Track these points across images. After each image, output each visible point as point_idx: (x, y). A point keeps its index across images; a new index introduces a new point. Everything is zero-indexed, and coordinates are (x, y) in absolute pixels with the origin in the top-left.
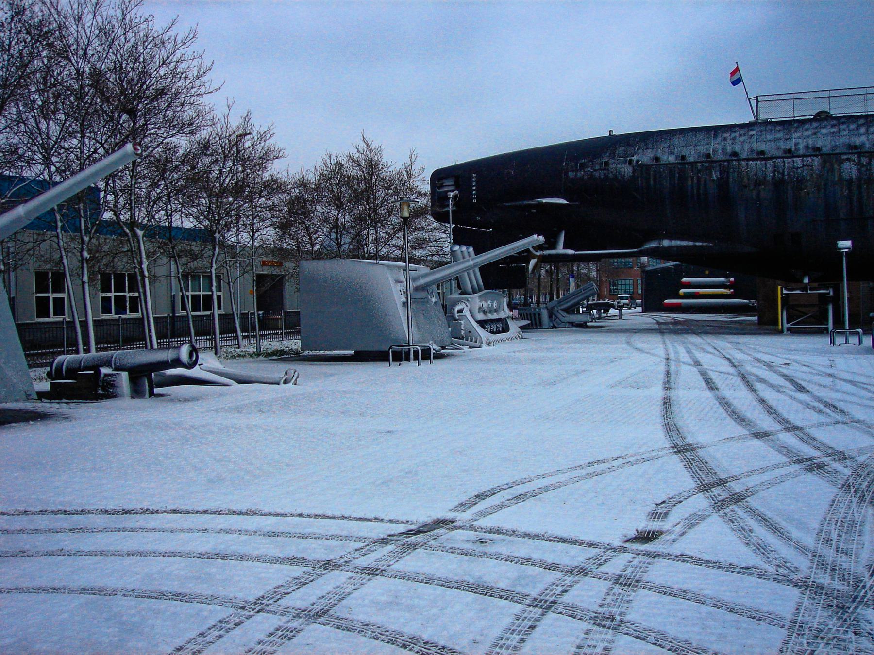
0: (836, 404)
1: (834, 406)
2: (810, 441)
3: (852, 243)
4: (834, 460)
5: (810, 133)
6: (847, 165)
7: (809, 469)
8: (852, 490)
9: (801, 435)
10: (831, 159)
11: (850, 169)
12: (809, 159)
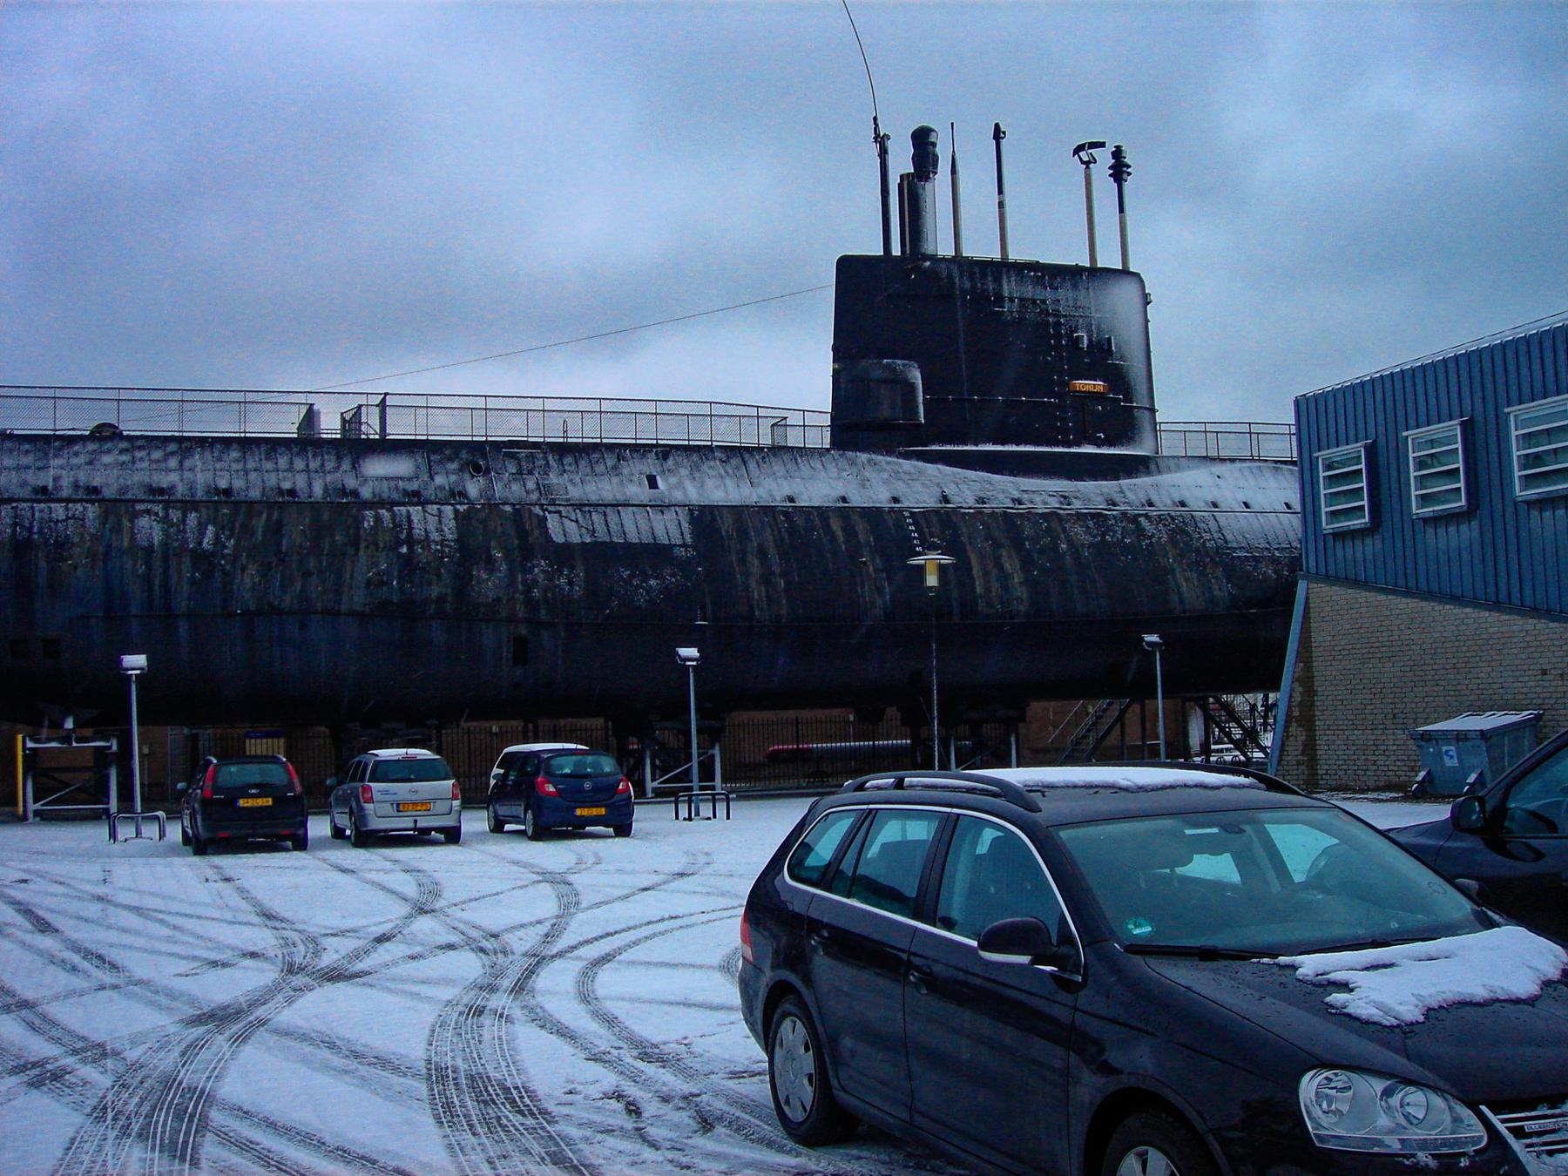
0: (104, 952)
1: (100, 957)
2: (46, 1027)
3: (121, 661)
4: (84, 1061)
5: (81, 460)
6: (144, 522)
7: (36, 1084)
8: (110, 1116)
9: (31, 1017)
10: (117, 508)
11: (149, 529)
12: (79, 507)
